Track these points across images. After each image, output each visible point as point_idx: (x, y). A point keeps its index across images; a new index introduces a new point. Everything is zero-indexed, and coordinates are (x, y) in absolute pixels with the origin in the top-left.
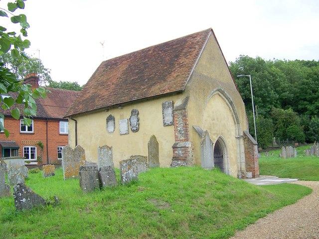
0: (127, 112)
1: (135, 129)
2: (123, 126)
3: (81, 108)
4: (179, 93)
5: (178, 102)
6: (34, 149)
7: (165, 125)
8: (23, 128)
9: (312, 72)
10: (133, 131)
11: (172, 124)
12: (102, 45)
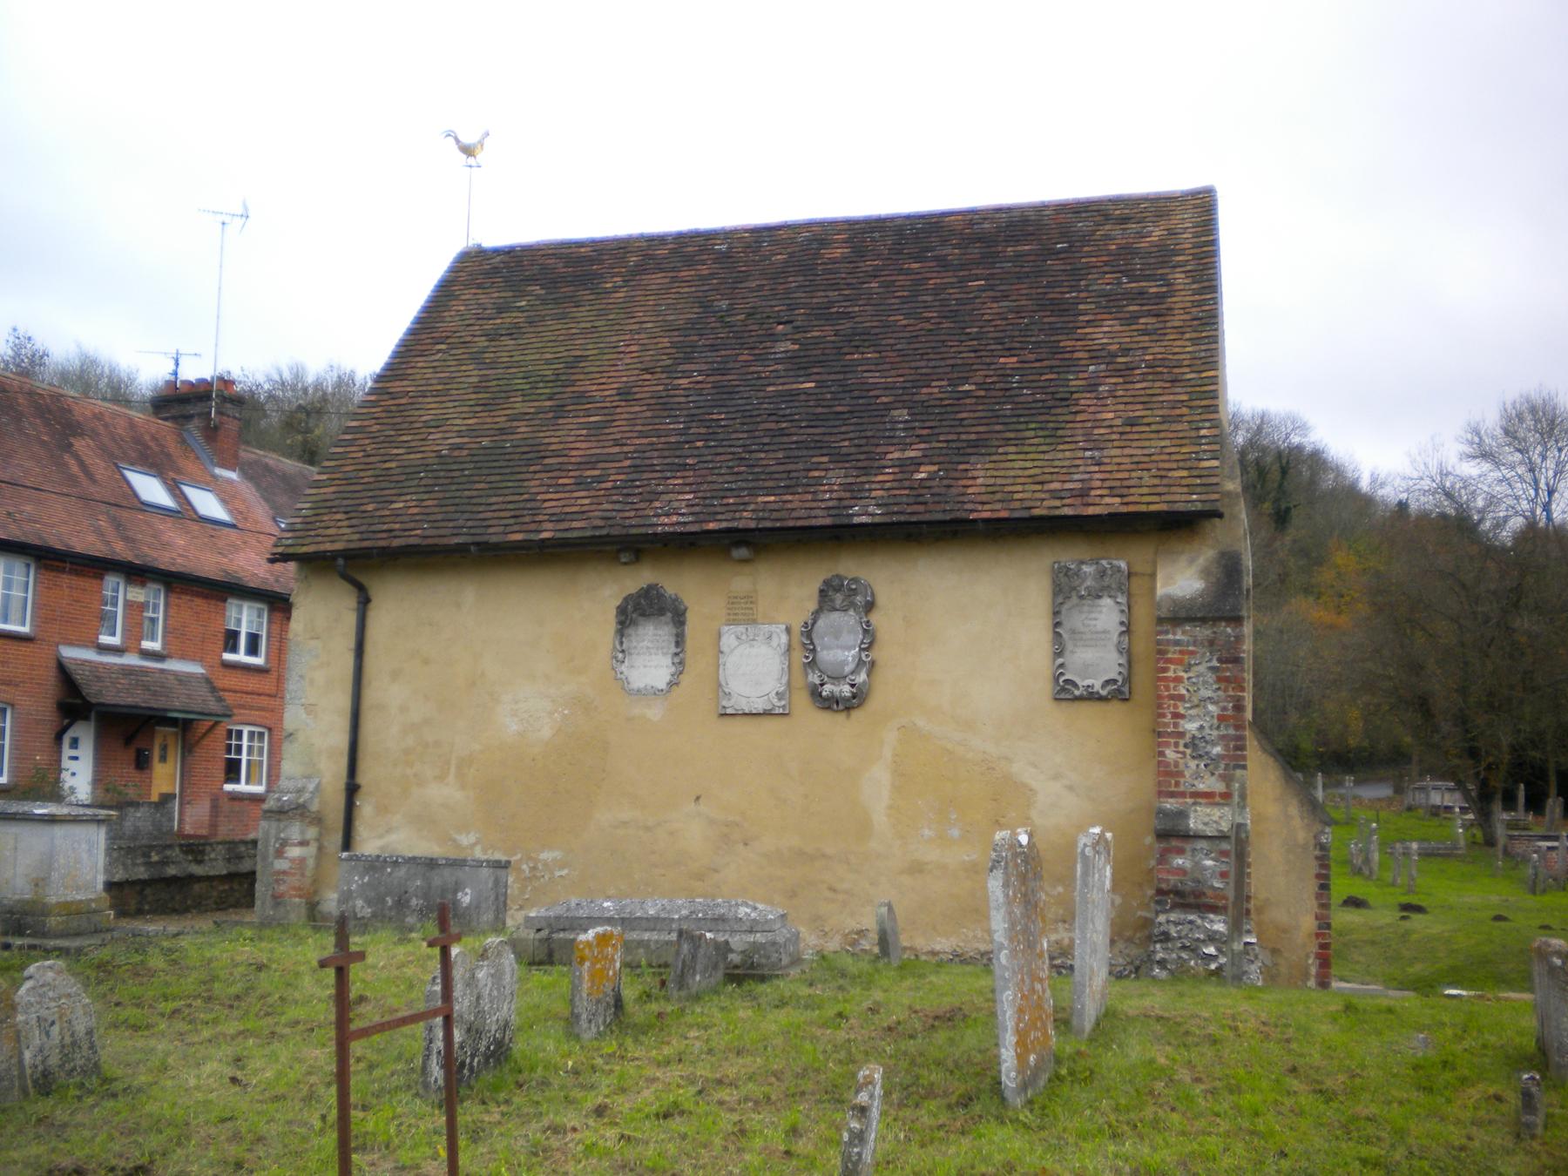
1: (846, 690)
6: (261, 735)
7: (1065, 692)
8: (231, 640)
10: (829, 704)
11: (1118, 693)
12: (468, 151)
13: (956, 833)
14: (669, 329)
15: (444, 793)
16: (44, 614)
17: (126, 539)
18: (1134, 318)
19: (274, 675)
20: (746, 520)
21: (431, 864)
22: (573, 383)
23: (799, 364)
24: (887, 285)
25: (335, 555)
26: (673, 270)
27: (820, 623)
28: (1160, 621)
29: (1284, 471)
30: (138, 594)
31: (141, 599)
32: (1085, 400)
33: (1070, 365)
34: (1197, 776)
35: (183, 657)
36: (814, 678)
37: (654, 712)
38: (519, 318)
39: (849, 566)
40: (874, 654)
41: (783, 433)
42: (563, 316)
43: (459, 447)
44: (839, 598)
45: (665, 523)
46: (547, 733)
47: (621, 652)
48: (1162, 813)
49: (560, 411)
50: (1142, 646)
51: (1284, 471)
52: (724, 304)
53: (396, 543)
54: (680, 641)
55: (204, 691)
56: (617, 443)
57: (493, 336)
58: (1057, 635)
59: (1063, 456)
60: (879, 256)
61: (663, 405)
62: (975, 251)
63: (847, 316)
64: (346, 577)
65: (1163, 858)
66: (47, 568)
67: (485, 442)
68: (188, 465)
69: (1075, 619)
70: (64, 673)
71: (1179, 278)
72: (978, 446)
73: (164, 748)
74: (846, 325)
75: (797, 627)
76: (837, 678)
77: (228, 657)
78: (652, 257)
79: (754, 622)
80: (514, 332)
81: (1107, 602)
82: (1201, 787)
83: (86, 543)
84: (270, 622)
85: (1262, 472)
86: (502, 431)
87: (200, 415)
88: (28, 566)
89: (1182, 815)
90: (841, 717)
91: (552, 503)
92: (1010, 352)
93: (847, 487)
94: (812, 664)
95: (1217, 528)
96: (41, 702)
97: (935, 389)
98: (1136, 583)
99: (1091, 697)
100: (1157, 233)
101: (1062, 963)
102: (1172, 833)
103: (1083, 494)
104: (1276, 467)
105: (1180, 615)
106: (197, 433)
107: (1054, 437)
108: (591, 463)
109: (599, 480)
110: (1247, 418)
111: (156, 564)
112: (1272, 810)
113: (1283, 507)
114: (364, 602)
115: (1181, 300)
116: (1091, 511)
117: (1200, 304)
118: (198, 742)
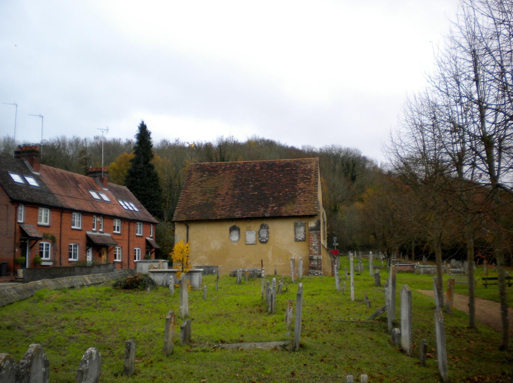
0: (256, 226)
1: (265, 240)
2: (251, 237)
3: (194, 214)
4: (311, 217)
5: (312, 224)
6: (48, 245)
7: (296, 240)
9: (305, 329)
10: (263, 242)
11: (304, 240)
13: (281, 260)
14: (232, 182)
15: (203, 257)
16: (84, 225)
17: (95, 207)
18: (306, 182)
19: (122, 235)
20: (249, 216)
21: (209, 267)
22: (217, 192)
23: (254, 189)
24: (267, 175)
25: (184, 221)
26: (230, 170)
27: (261, 231)
28: (309, 230)
29: (354, 165)
30: (98, 219)
31: (99, 220)
32: (298, 197)
33: (296, 191)
34: (315, 251)
35: (107, 232)
36: (260, 239)
37: (236, 244)
38: (205, 178)
39: (265, 222)
40: (269, 235)
41: (253, 201)
42: (213, 178)
43: (200, 203)
44: (263, 227)
45: (237, 216)
46: (219, 247)
47: (230, 235)
48: (310, 257)
49: (216, 197)
50: (307, 234)
51: (354, 165)
52: (240, 177)
53: (194, 219)
54: (239, 233)
55: (112, 240)
56: (227, 203)
57: (201, 182)
58: (295, 232)
59: (295, 206)
60: (265, 169)
61: (233, 196)
62: (281, 169)
63: (261, 180)
64: (185, 224)
65: (310, 263)
66: (84, 215)
67: (205, 202)
68: (99, 188)
69: (297, 230)
70: (88, 238)
71: (313, 175)
72: (283, 204)
73: (103, 252)
74: (261, 182)
75: (257, 231)
76: (263, 239)
77: (114, 232)
78: (227, 167)
79: (250, 231)
80: (205, 181)
81: (302, 227)
82: (315, 253)
83: (89, 209)
84: (121, 224)
85: (348, 165)
86: (207, 200)
87: (99, 176)
88: (80, 215)
89: (312, 257)
90: (264, 244)
91: (218, 213)
92: (287, 188)
93: (264, 211)
94: (260, 237)
95: (317, 217)
96: (82, 243)
97: (276, 194)
98: (306, 224)
99: (300, 241)
100: (309, 167)
101: (298, 272)
102: (311, 259)
103: (298, 212)
104: (352, 163)
105: (312, 229)
106: (98, 180)
107: (294, 203)
108: (223, 206)
109: (225, 209)
110: (343, 150)
111: (101, 213)
112: (325, 256)
113: (354, 175)
114: (188, 228)
115: (313, 179)
116: (300, 215)
117: (316, 180)
118: (110, 250)
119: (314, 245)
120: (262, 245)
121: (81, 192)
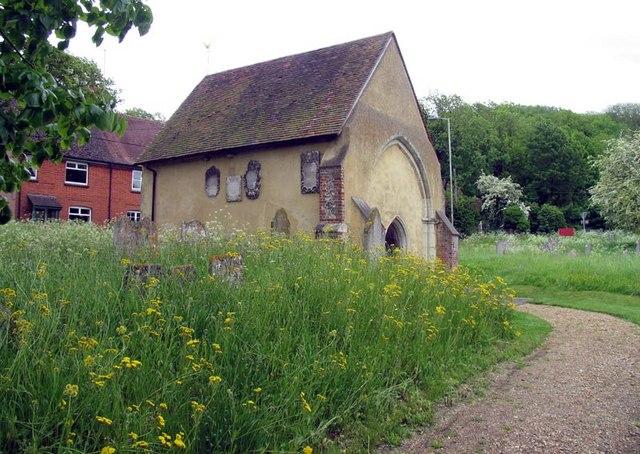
0: (241, 165)
7: (304, 191)
10: (250, 197)
119: (327, 200)
120: (249, 202)
121: (411, 158)
